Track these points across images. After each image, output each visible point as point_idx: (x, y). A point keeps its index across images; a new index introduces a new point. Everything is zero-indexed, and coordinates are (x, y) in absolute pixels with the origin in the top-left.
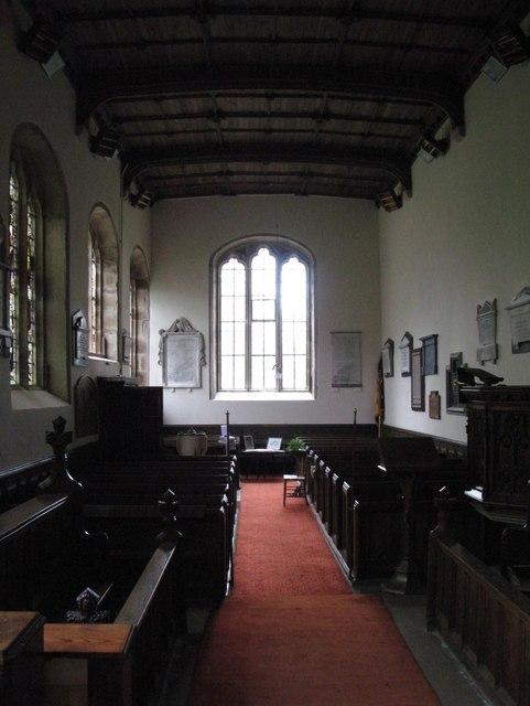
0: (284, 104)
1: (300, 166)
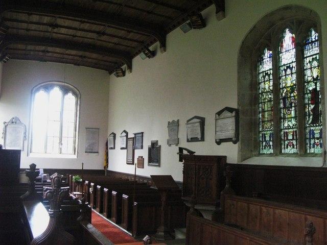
0: (86, 26)
1: (81, 53)
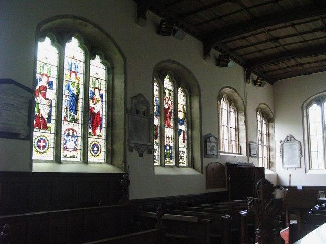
0: (302, 28)
